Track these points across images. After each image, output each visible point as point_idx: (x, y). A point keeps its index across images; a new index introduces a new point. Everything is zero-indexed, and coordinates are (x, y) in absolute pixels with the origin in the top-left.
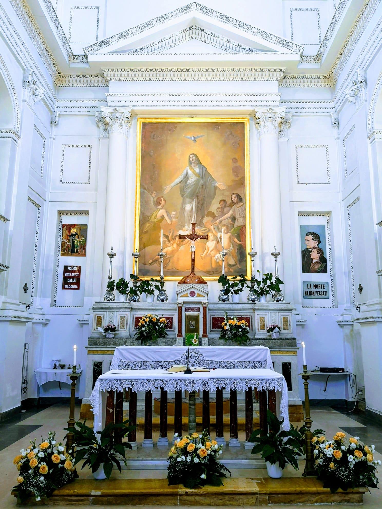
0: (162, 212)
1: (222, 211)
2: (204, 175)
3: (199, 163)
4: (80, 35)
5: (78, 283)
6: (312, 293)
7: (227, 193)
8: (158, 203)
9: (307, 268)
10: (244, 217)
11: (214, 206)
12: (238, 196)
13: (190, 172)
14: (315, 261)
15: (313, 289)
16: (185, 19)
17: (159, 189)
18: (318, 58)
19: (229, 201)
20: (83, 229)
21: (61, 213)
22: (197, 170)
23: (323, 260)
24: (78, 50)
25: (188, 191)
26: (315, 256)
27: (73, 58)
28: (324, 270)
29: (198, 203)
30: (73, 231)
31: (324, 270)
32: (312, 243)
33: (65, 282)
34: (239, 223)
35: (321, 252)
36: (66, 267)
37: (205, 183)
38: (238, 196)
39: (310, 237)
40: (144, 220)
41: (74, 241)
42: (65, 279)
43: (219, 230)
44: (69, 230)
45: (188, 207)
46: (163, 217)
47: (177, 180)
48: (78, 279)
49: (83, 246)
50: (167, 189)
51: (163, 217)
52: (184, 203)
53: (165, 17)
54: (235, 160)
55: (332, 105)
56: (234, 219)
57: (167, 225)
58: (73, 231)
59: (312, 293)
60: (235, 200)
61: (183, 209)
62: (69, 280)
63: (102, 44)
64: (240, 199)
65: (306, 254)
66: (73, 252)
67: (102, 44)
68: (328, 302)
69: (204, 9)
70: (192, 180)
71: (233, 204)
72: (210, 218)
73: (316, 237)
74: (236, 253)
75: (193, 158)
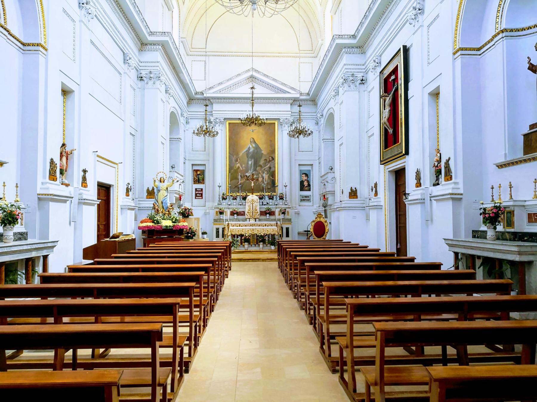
0: (238, 165)
1: (265, 164)
2: (257, 148)
3: (255, 142)
4: (198, 86)
5: (202, 196)
6: (304, 200)
7: (268, 156)
8: (237, 161)
9: (302, 188)
10: (275, 167)
11: (262, 162)
12: (272, 157)
13: (251, 146)
14: (305, 186)
15: (304, 198)
16: (250, 74)
17: (237, 154)
18: (308, 94)
19: (268, 160)
20: (203, 172)
21: (193, 165)
22: (254, 145)
23: (309, 185)
24: (198, 90)
25: (250, 155)
26: (306, 184)
27: (196, 93)
28: (310, 190)
29: (254, 161)
30: (199, 173)
31: (310, 190)
32: (305, 178)
33: (196, 196)
34: (272, 170)
35: (308, 182)
36: (196, 189)
37: (257, 151)
38: (272, 157)
39: (304, 175)
40: (231, 168)
41: (199, 177)
42: (196, 194)
43: (263, 173)
44: (197, 172)
45: (250, 163)
46: (239, 167)
47: (245, 150)
48: (202, 194)
49: (203, 180)
50: (241, 154)
51: (239, 167)
52: (248, 161)
53: (239, 75)
54: (271, 141)
55: (364, 71)
56: (270, 168)
57: (241, 171)
58: (199, 173)
59: (304, 200)
60: (271, 159)
61: (248, 163)
62: (198, 195)
63: (210, 88)
64: (273, 159)
65: (302, 183)
66: (199, 182)
67: (210, 88)
68: (310, 204)
69: (256, 71)
70: (251, 150)
71: (270, 161)
72: (260, 168)
73: (307, 175)
74: (271, 183)
75: (252, 140)
